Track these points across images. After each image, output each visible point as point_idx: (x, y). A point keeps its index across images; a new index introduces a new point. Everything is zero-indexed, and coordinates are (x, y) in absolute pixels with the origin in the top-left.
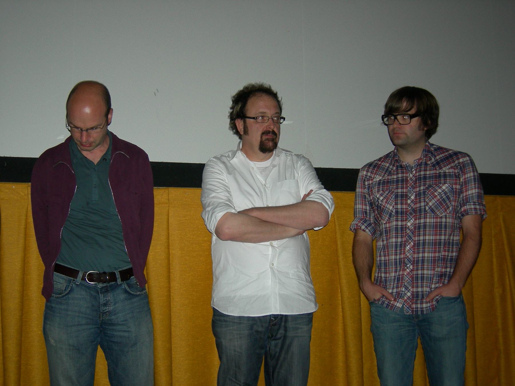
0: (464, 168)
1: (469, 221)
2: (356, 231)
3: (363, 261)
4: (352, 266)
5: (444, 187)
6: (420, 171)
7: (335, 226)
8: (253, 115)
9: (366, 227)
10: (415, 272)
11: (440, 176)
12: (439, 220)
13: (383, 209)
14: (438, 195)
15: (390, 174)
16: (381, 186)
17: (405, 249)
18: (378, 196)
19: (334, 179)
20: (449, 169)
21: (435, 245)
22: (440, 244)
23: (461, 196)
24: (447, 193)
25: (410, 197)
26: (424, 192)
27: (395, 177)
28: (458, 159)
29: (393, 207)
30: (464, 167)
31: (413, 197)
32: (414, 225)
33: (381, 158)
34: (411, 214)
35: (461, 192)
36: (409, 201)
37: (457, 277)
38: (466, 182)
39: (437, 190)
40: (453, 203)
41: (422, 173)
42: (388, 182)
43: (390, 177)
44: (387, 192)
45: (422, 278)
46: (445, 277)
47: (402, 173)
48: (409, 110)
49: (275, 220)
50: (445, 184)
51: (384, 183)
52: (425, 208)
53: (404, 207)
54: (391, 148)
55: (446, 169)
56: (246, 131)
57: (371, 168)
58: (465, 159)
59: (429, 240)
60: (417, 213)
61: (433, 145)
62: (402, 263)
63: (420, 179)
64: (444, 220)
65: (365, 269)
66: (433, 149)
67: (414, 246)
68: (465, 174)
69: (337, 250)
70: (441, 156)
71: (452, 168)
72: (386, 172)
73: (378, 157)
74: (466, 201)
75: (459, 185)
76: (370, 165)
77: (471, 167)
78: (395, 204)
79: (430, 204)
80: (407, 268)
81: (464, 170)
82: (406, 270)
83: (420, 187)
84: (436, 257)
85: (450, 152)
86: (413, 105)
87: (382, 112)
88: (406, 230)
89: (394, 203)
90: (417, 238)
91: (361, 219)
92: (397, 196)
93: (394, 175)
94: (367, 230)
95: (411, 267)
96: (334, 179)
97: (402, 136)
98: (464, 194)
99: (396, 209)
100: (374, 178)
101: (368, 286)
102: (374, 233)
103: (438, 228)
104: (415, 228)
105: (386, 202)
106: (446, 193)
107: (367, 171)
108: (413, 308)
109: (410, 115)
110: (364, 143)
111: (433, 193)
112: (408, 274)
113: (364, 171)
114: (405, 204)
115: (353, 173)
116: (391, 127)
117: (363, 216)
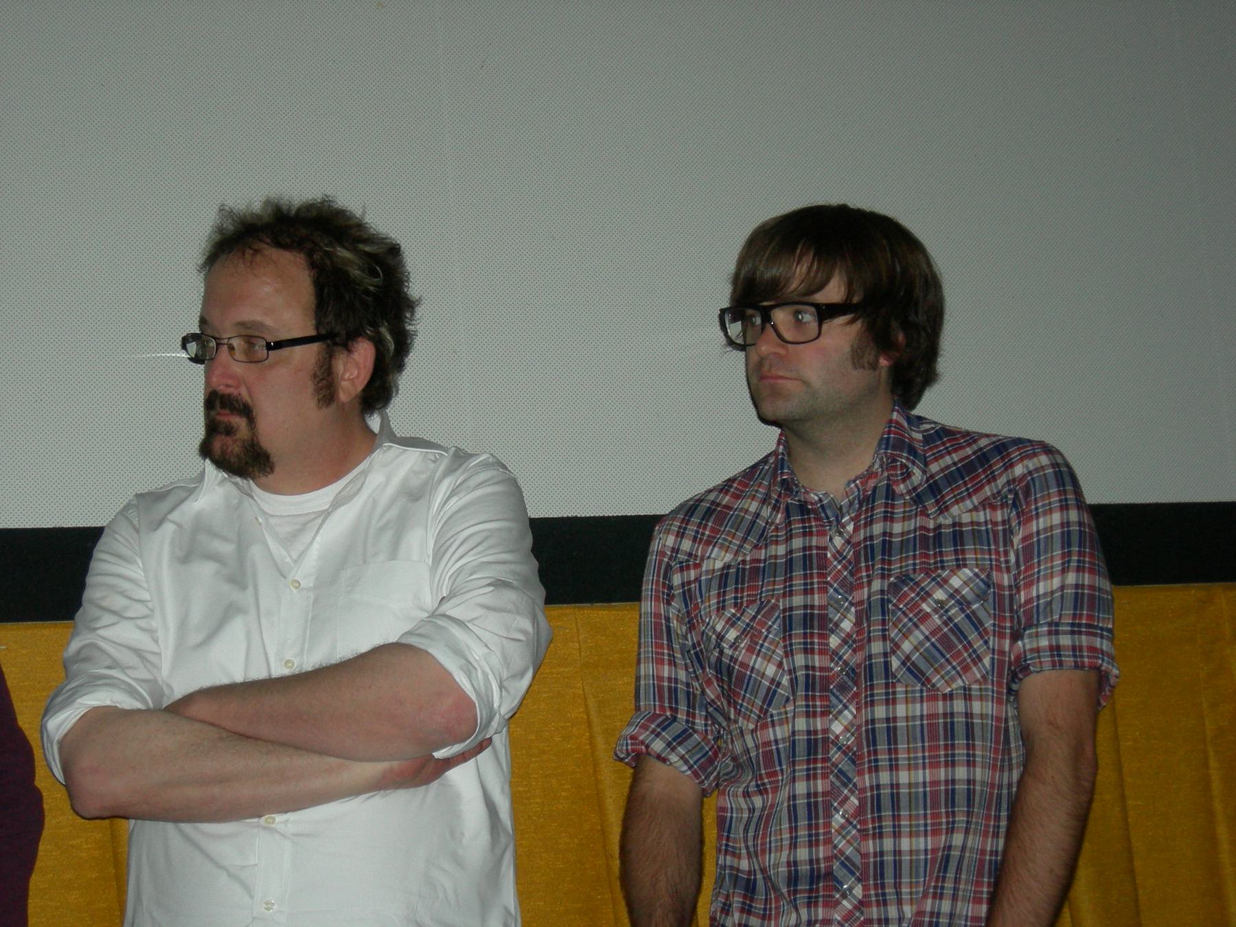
2: (638, 760)
5: (956, 582)
6: (870, 522)
7: (591, 737)
9: (669, 744)
12: (940, 707)
13: (741, 677)
14: (936, 611)
15: (764, 540)
17: (828, 825)
18: (719, 628)
20: (975, 509)
22: (951, 796)
24: (969, 604)
25: (837, 625)
26: (883, 603)
29: (780, 665)
30: (1027, 493)
31: (847, 625)
33: (730, 481)
34: (843, 688)
36: (834, 641)
39: (929, 595)
41: (878, 528)
42: (755, 572)
44: (751, 612)
48: (820, 287)
50: (959, 567)
51: (740, 576)
52: (887, 665)
53: (817, 661)
55: (962, 512)
57: (695, 520)
58: (1031, 464)
59: (910, 785)
61: (920, 419)
67: (860, 810)
70: (948, 460)
71: (985, 504)
72: (748, 532)
73: (718, 479)
76: (689, 509)
77: (1054, 490)
79: (907, 646)
80: (844, 896)
82: (838, 903)
85: (983, 442)
86: (849, 274)
87: (723, 297)
88: (826, 751)
89: (780, 651)
91: (654, 717)
92: (787, 626)
93: (777, 543)
94: (674, 758)
95: (858, 891)
96: (581, 561)
97: (790, 385)
100: (702, 559)
103: (944, 735)
105: (750, 649)
106: (963, 604)
107: (681, 535)
109: (817, 306)
110: (668, 423)
111: (917, 605)
114: (821, 652)
117: (662, 708)
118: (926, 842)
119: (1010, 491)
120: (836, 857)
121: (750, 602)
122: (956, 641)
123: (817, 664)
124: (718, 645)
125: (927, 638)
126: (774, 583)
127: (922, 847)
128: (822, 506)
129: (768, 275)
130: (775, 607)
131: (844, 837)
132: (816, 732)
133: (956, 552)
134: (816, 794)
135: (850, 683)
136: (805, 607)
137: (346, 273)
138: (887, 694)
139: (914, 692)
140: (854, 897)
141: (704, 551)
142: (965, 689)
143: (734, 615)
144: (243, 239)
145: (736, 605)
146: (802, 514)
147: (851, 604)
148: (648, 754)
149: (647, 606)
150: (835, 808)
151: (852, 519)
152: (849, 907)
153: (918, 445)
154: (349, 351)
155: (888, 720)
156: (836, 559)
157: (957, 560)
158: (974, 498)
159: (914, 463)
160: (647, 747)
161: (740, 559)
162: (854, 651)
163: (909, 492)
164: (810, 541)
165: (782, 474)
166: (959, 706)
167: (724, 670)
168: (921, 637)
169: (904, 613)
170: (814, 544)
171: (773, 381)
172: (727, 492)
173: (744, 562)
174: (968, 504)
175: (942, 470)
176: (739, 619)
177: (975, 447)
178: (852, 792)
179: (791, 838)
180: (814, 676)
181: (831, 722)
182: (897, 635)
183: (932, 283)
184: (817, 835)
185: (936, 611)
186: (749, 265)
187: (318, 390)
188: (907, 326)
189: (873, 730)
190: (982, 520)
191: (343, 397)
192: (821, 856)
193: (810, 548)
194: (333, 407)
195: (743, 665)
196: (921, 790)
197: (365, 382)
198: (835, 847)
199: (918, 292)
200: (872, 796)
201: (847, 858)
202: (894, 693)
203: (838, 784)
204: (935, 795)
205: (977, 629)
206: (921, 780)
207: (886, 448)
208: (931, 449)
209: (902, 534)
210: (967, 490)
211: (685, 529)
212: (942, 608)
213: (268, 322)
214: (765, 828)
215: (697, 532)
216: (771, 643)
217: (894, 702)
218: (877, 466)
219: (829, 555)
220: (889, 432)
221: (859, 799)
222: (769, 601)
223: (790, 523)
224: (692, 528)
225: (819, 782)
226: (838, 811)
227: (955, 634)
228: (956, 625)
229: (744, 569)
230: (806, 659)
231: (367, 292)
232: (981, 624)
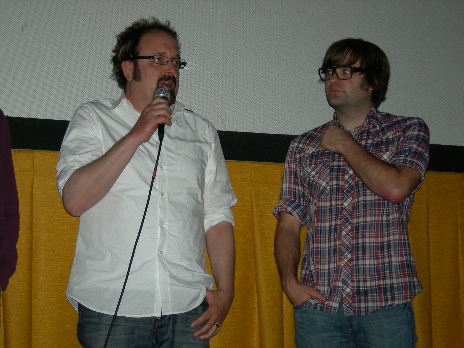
3: (287, 255)
4: (273, 259)
7: (252, 206)
9: (293, 209)
10: (354, 263)
17: (340, 234)
25: (348, 172)
29: (327, 183)
33: (318, 128)
34: (348, 192)
36: (346, 177)
44: (320, 166)
50: (386, 151)
54: (328, 114)
56: (137, 76)
62: (337, 253)
65: (291, 262)
67: (352, 230)
69: (253, 238)
73: (314, 127)
76: (303, 136)
78: (330, 180)
80: (345, 258)
82: (342, 260)
86: (360, 63)
87: (320, 64)
90: (355, 221)
92: (332, 170)
94: (294, 213)
95: (349, 256)
97: (340, 94)
99: (330, 186)
101: (292, 286)
104: (353, 209)
105: (319, 178)
108: (355, 307)
110: (295, 105)
114: (342, 180)
116: (329, 83)
120: (342, 245)
121: (320, 163)
124: (308, 176)
126: (329, 158)
129: (335, 58)
130: (328, 165)
132: (338, 205)
134: (337, 225)
140: (348, 258)
141: (307, 147)
144: (340, 47)
145: (315, 164)
148: (286, 212)
149: (287, 165)
160: (286, 209)
162: (353, 180)
170: (342, 165)
171: (334, 92)
172: (316, 132)
173: (319, 151)
178: (349, 224)
181: (344, 202)
183: (387, 66)
198: (342, 241)
201: (346, 245)
204: (378, 224)
214: (168, 111)
218: (365, 124)
221: (351, 227)
230: (337, 182)
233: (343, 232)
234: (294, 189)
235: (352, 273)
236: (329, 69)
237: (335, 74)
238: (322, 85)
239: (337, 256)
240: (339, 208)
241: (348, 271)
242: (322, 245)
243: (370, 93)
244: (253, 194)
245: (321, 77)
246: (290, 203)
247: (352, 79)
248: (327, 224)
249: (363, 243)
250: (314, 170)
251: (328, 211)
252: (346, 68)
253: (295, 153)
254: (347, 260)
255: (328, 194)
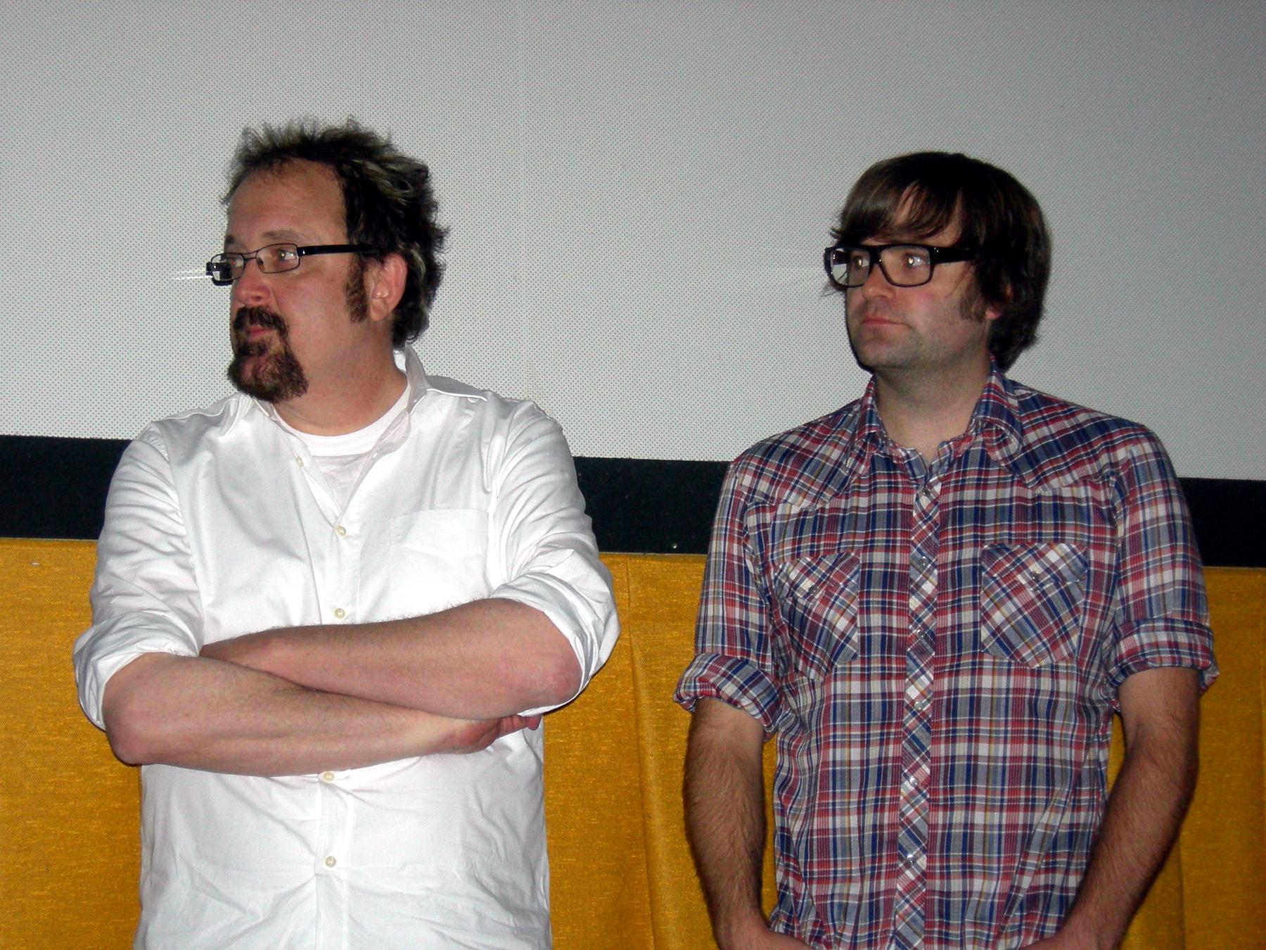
0: (1131, 483)
1: (1149, 693)
2: (698, 708)
3: (727, 834)
5: (1053, 556)
6: (961, 487)
7: (636, 691)
8: (341, 247)
9: (741, 688)
11: (1037, 511)
13: (814, 627)
15: (844, 489)
16: (807, 535)
17: (896, 791)
18: (793, 576)
19: (637, 507)
20: (1076, 484)
21: (1015, 779)
23: (1118, 597)
24: (1064, 580)
25: (918, 586)
26: (975, 571)
27: (863, 502)
28: (1111, 448)
29: (853, 620)
31: (928, 587)
32: (934, 696)
33: (811, 425)
34: (921, 652)
35: (1118, 580)
36: (914, 603)
37: (1091, 911)
38: (1136, 542)
40: (1085, 620)
41: (969, 494)
43: (842, 504)
44: (828, 562)
45: (971, 773)
46: (1047, 908)
47: (890, 490)
49: (357, 684)
50: (1056, 541)
51: (818, 524)
52: (976, 634)
53: (895, 622)
55: (1064, 485)
57: (774, 461)
58: (1136, 450)
59: (989, 758)
60: (949, 650)
61: (1015, 385)
62: (884, 847)
63: (959, 516)
64: (1046, 683)
66: (1014, 402)
67: (931, 780)
68: (1134, 510)
69: (643, 790)
70: (1045, 431)
71: (1085, 480)
73: (799, 421)
74: (1137, 616)
75: (1112, 549)
76: (767, 449)
77: (1157, 480)
78: (861, 611)
79: (998, 617)
80: (908, 865)
81: (1133, 493)
82: (901, 872)
83: (959, 546)
84: (1015, 827)
85: (1082, 418)
86: (957, 226)
88: (900, 716)
89: (855, 607)
90: (942, 750)
91: (723, 660)
93: (859, 494)
94: (745, 701)
95: (923, 862)
96: (637, 507)
97: (894, 331)
98: (1131, 588)
100: (778, 503)
102: (772, 709)
104: (936, 706)
105: (825, 601)
106: (1058, 579)
107: (758, 475)
109: (930, 248)
110: (746, 356)
111: (1010, 576)
112: (910, 887)
113: (745, 471)
114: (900, 613)
115: (701, 481)
116: (857, 297)
118: (1001, 817)
119: (1112, 474)
120: (902, 825)
121: (827, 552)
122: (1048, 617)
123: (895, 625)
124: (791, 594)
125: (1019, 610)
127: (996, 822)
128: (910, 463)
130: (854, 561)
131: (913, 806)
133: (1056, 526)
134: (886, 759)
135: (928, 647)
136: (886, 565)
137: (374, 187)
138: (974, 664)
139: (1001, 664)
140: (918, 867)
141: (781, 493)
142: (1052, 666)
143: (809, 564)
144: (267, 158)
145: (812, 554)
146: (888, 469)
147: (934, 566)
148: (719, 697)
150: (905, 775)
151: (940, 480)
152: (912, 877)
153: (1015, 412)
154: (383, 262)
155: (972, 690)
156: (921, 518)
157: (1056, 534)
158: (1074, 472)
159: (1012, 431)
160: (718, 690)
161: (819, 506)
162: (935, 614)
163: (1005, 460)
164: (896, 497)
165: (870, 427)
166: (1046, 683)
167: (797, 622)
168: (1014, 610)
169: (997, 582)
170: (899, 501)
171: (877, 325)
172: (807, 438)
173: (823, 510)
174: (1069, 478)
175: (1040, 440)
176: (814, 568)
177: (1073, 421)
179: (859, 802)
180: (890, 638)
181: (907, 686)
182: (988, 604)
183: (1041, 239)
184: (883, 800)
185: (1031, 583)
186: (860, 200)
187: (351, 303)
188: (1017, 279)
189: (956, 700)
190: (1083, 496)
191: (374, 315)
192: (886, 822)
193: (895, 505)
194: (365, 322)
195: (816, 616)
196: (1000, 764)
197: (398, 300)
198: (903, 814)
199: (1030, 247)
200: (946, 767)
201: (914, 827)
202: (981, 663)
203: (910, 749)
205: (1069, 606)
206: (1001, 754)
207: (985, 414)
208: (1028, 417)
209: (996, 501)
210: (1066, 464)
211: (763, 469)
212: (1037, 581)
213: (297, 229)
215: (775, 474)
216: (846, 597)
217: (981, 672)
219: (914, 514)
220: (988, 397)
221: (931, 768)
222: (848, 554)
223: (875, 477)
224: (770, 469)
225: (891, 746)
226: (907, 777)
227: (1047, 609)
228: (1049, 600)
229: (822, 518)
231: (399, 206)
232: (1074, 601)
233: (906, 783)
234: (741, 622)
235: (927, 915)
236: (856, 253)
237: (877, 268)
238: (838, 299)
239: (881, 857)
240: (891, 703)
241: (915, 909)
242: (838, 819)
243: (987, 325)
244: (637, 655)
245: (831, 277)
246: (729, 668)
247: (931, 284)
248: (856, 754)
249: (966, 826)
250: (808, 574)
251: (856, 712)
252: (912, 251)
253: (745, 508)
254: (913, 873)
255: (855, 656)
